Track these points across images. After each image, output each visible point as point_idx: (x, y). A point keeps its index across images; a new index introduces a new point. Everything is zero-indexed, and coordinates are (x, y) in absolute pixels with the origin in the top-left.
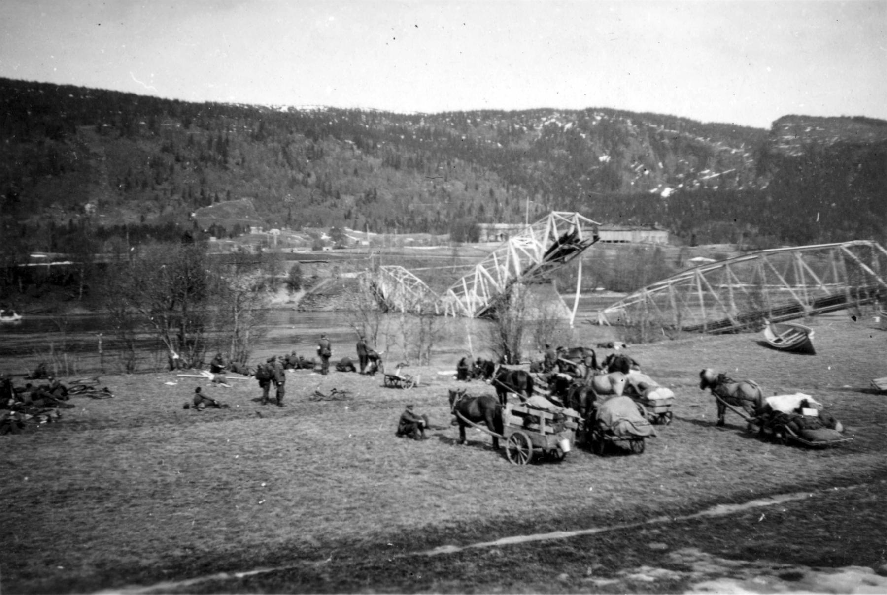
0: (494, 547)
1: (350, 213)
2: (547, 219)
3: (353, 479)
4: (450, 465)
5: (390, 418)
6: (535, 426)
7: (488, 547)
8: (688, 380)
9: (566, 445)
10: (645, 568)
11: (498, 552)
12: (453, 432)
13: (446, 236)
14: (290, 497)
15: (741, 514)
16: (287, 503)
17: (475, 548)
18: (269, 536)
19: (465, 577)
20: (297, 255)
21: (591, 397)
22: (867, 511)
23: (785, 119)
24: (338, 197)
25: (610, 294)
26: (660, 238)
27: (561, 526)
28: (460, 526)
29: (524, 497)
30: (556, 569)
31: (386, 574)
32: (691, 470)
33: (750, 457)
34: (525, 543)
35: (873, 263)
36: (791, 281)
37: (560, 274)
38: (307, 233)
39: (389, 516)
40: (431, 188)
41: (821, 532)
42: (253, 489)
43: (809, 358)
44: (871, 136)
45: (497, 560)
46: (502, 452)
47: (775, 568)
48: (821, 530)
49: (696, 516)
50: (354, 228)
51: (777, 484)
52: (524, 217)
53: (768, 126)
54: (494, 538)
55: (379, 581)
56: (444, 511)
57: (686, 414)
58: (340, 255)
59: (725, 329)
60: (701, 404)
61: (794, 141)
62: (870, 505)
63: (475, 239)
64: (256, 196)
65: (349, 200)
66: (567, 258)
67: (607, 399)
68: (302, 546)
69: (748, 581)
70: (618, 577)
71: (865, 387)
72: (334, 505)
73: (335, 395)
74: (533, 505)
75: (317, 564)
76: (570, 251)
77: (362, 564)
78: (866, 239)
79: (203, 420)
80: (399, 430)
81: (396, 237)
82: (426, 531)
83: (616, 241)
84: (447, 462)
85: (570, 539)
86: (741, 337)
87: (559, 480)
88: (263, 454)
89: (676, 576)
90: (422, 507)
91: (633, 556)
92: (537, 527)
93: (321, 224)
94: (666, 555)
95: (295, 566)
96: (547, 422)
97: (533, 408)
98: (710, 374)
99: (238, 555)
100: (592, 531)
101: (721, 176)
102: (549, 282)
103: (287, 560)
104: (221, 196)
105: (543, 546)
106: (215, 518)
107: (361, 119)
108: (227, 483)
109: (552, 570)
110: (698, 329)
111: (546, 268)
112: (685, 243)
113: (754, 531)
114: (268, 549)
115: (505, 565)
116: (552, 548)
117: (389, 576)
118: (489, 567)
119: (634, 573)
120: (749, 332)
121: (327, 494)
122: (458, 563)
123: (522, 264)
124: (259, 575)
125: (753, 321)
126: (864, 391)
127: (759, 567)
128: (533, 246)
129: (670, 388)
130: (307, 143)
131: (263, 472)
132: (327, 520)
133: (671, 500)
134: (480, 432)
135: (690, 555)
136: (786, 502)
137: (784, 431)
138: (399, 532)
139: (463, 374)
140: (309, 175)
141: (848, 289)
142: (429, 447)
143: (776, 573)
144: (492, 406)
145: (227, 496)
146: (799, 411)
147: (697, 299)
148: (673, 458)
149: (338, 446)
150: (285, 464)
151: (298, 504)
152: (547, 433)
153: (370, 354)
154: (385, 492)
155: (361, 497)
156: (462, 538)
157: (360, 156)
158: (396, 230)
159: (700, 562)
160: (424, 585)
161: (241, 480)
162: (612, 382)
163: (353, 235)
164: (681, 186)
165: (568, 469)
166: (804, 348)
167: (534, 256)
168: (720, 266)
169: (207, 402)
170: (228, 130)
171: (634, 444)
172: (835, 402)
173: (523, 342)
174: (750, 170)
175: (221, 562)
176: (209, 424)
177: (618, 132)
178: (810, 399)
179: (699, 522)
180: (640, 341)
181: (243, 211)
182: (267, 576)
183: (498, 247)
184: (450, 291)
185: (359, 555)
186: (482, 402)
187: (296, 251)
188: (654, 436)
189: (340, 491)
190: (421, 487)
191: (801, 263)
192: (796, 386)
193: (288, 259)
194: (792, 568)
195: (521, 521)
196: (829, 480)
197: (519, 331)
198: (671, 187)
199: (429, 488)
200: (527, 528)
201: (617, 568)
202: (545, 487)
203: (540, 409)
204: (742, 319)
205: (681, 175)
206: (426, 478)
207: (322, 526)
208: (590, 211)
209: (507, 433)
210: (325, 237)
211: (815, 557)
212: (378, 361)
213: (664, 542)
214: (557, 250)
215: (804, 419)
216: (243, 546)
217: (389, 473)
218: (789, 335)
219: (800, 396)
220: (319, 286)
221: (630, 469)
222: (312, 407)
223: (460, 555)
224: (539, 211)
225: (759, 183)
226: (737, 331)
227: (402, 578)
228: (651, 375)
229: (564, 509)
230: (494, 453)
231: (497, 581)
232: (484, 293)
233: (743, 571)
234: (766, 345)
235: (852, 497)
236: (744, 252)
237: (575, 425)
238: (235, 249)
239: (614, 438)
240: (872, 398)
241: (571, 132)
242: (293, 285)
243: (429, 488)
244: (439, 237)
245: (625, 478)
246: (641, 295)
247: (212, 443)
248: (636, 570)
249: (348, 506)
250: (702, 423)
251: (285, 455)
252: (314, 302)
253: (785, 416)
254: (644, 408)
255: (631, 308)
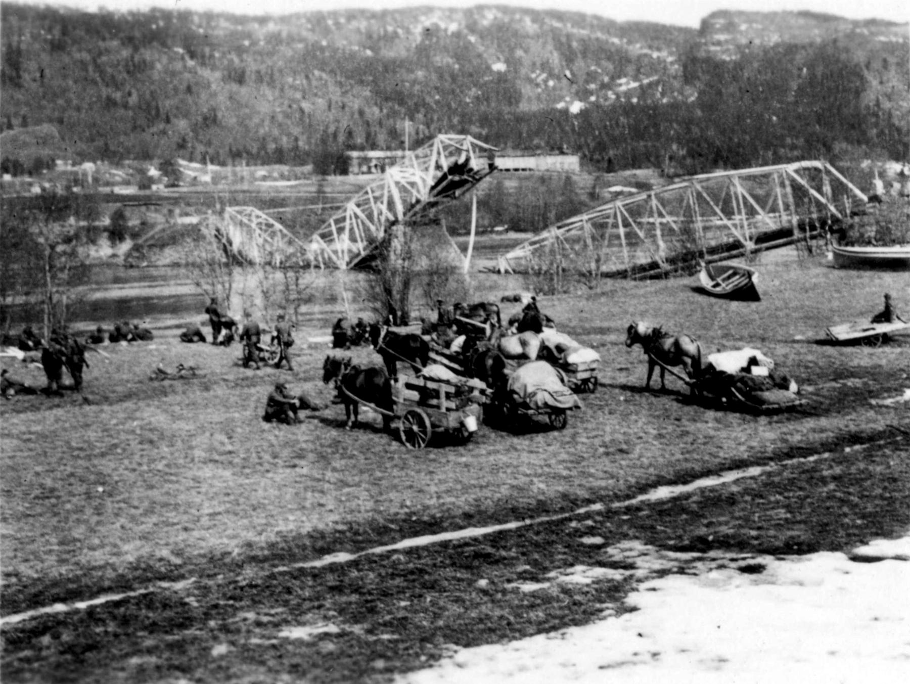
0: (395, 551)
1: (184, 140)
2: (432, 145)
3: (214, 477)
4: (333, 453)
5: (254, 399)
6: (434, 402)
7: (389, 552)
8: (612, 337)
9: (472, 424)
10: (579, 568)
11: (402, 557)
12: (337, 412)
13: (309, 168)
14: (136, 503)
15: (687, 496)
16: (133, 511)
17: (373, 554)
18: (115, 554)
19: (365, 590)
20: (118, 195)
21: (499, 365)
22: (832, 486)
23: (714, 15)
24: (168, 121)
25: (513, 235)
26: (570, 164)
27: (474, 521)
28: (351, 528)
29: (426, 488)
30: (473, 574)
31: (268, 593)
32: (624, 447)
33: (691, 427)
34: (434, 544)
35: (824, 189)
36: (728, 212)
37: (449, 212)
38: (130, 167)
39: (264, 521)
40: (285, 108)
41: (782, 513)
42: (88, 496)
43: (754, 305)
44: (817, 35)
45: (401, 567)
46: (395, 435)
47: (733, 560)
48: (783, 511)
49: (634, 502)
50: (191, 160)
51: (725, 459)
52: (403, 142)
53: (695, 24)
54: (394, 541)
55: (260, 602)
56: (331, 511)
57: (614, 378)
58: (176, 195)
59: (652, 272)
60: (629, 366)
61: (727, 41)
62: (835, 478)
63: (345, 172)
64: (61, 121)
65: (182, 124)
66: (457, 193)
67: (520, 365)
68: (158, 564)
69: (703, 577)
70: (548, 580)
71: (818, 338)
72: (194, 511)
73: (183, 372)
74: (439, 497)
75: (179, 586)
76: (462, 183)
77: (236, 582)
78: (816, 159)
79: (14, 410)
80: (267, 413)
81: (243, 170)
82: (312, 537)
83: (516, 170)
84: (329, 450)
85: (485, 536)
86: (672, 282)
87: (467, 465)
88: (97, 451)
89: (617, 575)
90: (304, 507)
91: (565, 553)
92: (445, 524)
93: (146, 156)
94: (603, 550)
95: (151, 589)
96: (448, 396)
97: (431, 379)
98: (643, 328)
99: (77, 579)
100: (512, 525)
101: (641, 87)
102: (436, 222)
103: (140, 583)
104: (15, 122)
105: (455, 547)
106: (42, 535)
107: (192, 21)
108: (52, 490)
109: (469, 576)
110: (622, 275)
111: (432, 205)
112: (599, 169)
113: (703, 516)
114: (115, 570)
115: (412, 572)
116: (467, 549)
117: (272, 595)
118: (393, 576)
119: (567, 575)
120: (681, 276)
121: (182, 498)
122: (354, 574)
123: (404, 201)
124: (107, 605)
125: (686, 262)
126: (820, 343)
127: (714, 560)
128: (417, 179)
129: (593, 347)
130: (125, 53)
131: (100, 474)
132: (186, 529)
133: (603, 483)
134: (368, 412)
135: (631, 550)
136: (738, 480)
137: (731, 395)
138: (279, 539)
139: (340, 340)
140: (130, 94)
141: (795, 220)
142: (304, 432)
143: (734, 565)
144: (380, 381)
145: (54, 506)
146: (747, 370)
147: (618, 237)
148: (601, 433)
149: (191, 436)
150: (126, 462)
151: (149, 512)
152: (448, 409)
153: (223, 320)
154: (256, 490)
155: (226, 499)
156: (355, 542)
157: (194, 67)
158: (244, 162)
159: (643, 558)
160: (316, 604)
161: (70, 485)
162: (524, 344)
163: (189, 169)
164: (593, 99)
165: (476, 451)
166: (747, 293)
167: (418, 191)
168: (644, 196)
169: (17, 387)
170: (20, 36)
171: (554, 419)
172: (786, 356)
173: (411, 298)
174: (675, 78)
175: (55, 591)
176: (22, 416)
177: (516, 34)
178: (760, 356)
179: (638, 509)
180: (552, 291)
181: (44, 141)
182: (117, 604)
183: (374, 180)
184: (316, 237)
185: (230, 571)
186: (372, 372)
187: (118, 190)
188: (577, 407)
189: (199, 493)
190: (300, 482)
191: (740, 189)
192: (741, 339)
193: (108, 202)
194: (753, 558)
195: (426, 518)
196: (785, 451)
197: (406, 284)
198: (581, 100)
199: (309, 483)
200: (433, 526)
201: (546, 570)
202: (451, 475)
203: (439, 381)
204: (671, 261)
205: (592, 86)
206: (305, 471)
207: (180, 538)
208: (484, 132)
209: (400, 410)
210: (153, 172)
211: (778, 543)
212: (234, 328)
213: (600, 535)
214: (444, 183)
215: (752, 379)
216: (81, 569)
217: (259, 467)
218: (729, 277)
219: (748, 352)
220: (151, 233)
221: (551, 448)
222: (154, 389)
223: (355, 564)
224: (421, 136)
225: (686, 93)
226: (666, 275)
227: (287, 597)
228: (569, 333)
229: (476, 500)
230: (384, 435)
231: (404, 593)
232: (359, 239)
233: (695, 564)
234: (700, 290)
235: (814, 470)
236: (670, 178)
237: (484, 399)
238: (36, 190)
239: (531, 412)
240: (829, 350)
241: (457, 35)
242: (116, 234)
243: (309, 483)
244: (299, 170)
245: (545, 460)
246: (551, 235)
247: (29, 440)
248: (569, 570)
249: (211, 511)
250: (633, 389)
251: (124, 450)
252: (144, 256)
253: (731, 377)
254: (564, 374)
255: (538, 253)
